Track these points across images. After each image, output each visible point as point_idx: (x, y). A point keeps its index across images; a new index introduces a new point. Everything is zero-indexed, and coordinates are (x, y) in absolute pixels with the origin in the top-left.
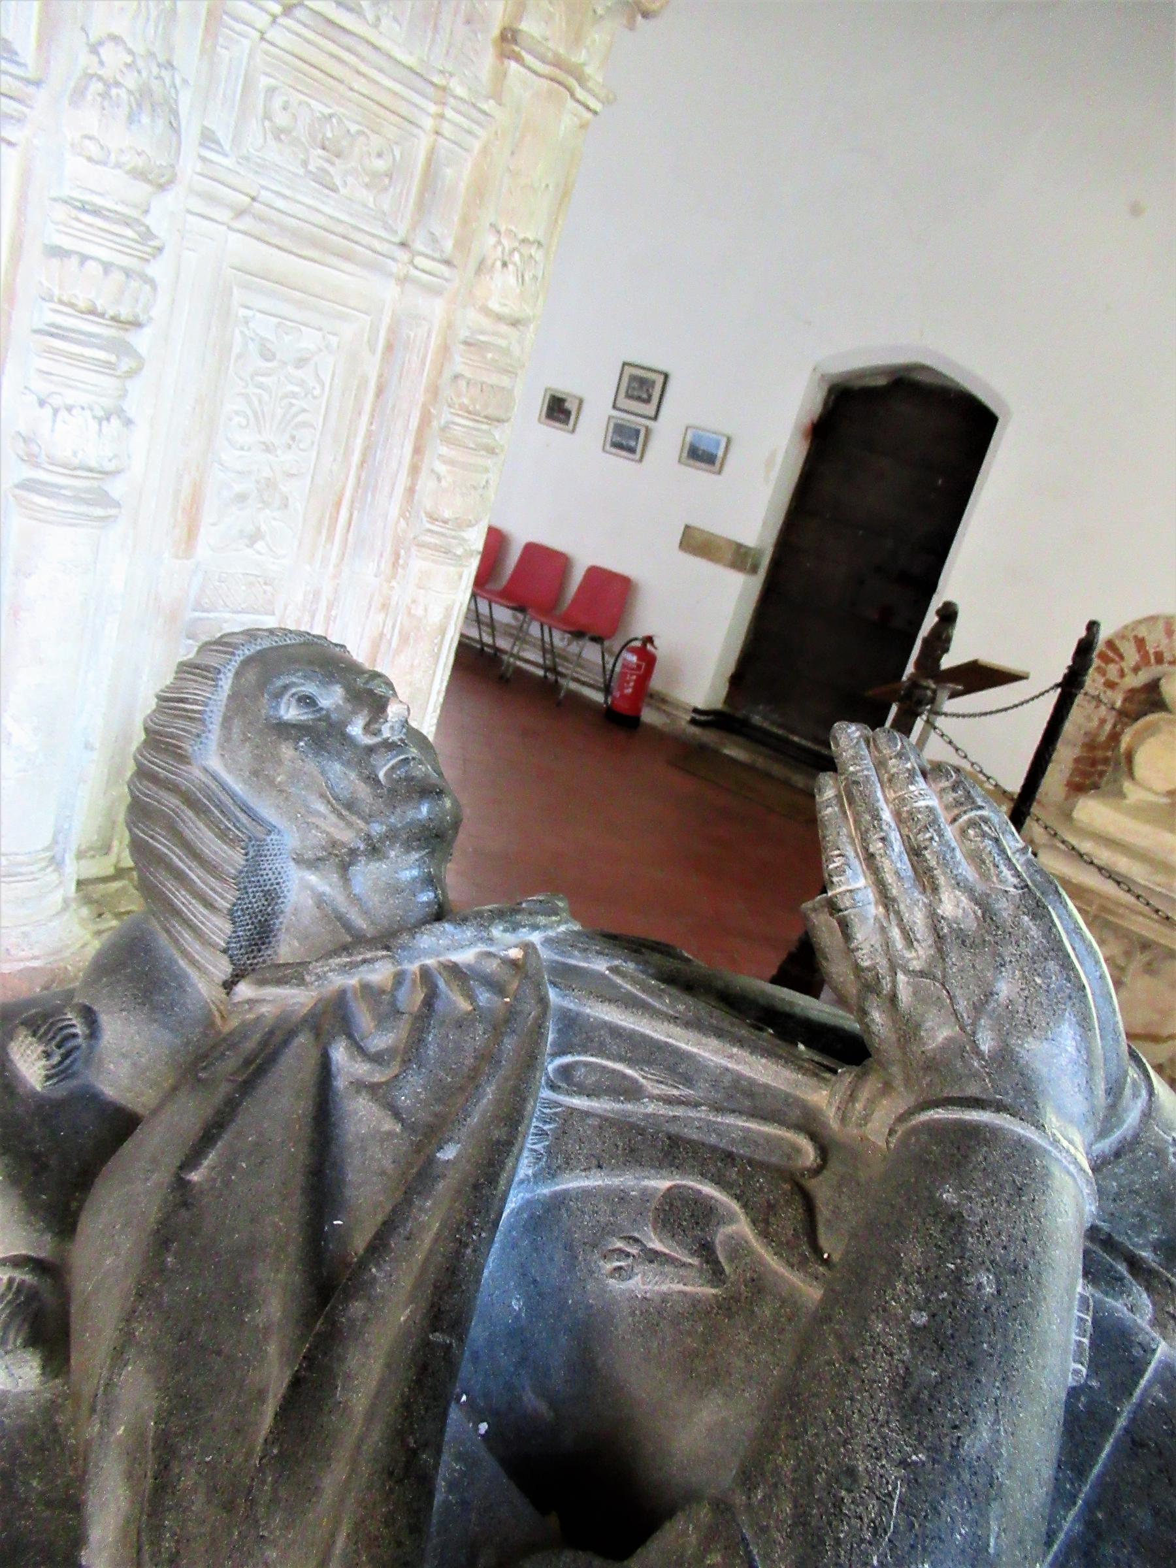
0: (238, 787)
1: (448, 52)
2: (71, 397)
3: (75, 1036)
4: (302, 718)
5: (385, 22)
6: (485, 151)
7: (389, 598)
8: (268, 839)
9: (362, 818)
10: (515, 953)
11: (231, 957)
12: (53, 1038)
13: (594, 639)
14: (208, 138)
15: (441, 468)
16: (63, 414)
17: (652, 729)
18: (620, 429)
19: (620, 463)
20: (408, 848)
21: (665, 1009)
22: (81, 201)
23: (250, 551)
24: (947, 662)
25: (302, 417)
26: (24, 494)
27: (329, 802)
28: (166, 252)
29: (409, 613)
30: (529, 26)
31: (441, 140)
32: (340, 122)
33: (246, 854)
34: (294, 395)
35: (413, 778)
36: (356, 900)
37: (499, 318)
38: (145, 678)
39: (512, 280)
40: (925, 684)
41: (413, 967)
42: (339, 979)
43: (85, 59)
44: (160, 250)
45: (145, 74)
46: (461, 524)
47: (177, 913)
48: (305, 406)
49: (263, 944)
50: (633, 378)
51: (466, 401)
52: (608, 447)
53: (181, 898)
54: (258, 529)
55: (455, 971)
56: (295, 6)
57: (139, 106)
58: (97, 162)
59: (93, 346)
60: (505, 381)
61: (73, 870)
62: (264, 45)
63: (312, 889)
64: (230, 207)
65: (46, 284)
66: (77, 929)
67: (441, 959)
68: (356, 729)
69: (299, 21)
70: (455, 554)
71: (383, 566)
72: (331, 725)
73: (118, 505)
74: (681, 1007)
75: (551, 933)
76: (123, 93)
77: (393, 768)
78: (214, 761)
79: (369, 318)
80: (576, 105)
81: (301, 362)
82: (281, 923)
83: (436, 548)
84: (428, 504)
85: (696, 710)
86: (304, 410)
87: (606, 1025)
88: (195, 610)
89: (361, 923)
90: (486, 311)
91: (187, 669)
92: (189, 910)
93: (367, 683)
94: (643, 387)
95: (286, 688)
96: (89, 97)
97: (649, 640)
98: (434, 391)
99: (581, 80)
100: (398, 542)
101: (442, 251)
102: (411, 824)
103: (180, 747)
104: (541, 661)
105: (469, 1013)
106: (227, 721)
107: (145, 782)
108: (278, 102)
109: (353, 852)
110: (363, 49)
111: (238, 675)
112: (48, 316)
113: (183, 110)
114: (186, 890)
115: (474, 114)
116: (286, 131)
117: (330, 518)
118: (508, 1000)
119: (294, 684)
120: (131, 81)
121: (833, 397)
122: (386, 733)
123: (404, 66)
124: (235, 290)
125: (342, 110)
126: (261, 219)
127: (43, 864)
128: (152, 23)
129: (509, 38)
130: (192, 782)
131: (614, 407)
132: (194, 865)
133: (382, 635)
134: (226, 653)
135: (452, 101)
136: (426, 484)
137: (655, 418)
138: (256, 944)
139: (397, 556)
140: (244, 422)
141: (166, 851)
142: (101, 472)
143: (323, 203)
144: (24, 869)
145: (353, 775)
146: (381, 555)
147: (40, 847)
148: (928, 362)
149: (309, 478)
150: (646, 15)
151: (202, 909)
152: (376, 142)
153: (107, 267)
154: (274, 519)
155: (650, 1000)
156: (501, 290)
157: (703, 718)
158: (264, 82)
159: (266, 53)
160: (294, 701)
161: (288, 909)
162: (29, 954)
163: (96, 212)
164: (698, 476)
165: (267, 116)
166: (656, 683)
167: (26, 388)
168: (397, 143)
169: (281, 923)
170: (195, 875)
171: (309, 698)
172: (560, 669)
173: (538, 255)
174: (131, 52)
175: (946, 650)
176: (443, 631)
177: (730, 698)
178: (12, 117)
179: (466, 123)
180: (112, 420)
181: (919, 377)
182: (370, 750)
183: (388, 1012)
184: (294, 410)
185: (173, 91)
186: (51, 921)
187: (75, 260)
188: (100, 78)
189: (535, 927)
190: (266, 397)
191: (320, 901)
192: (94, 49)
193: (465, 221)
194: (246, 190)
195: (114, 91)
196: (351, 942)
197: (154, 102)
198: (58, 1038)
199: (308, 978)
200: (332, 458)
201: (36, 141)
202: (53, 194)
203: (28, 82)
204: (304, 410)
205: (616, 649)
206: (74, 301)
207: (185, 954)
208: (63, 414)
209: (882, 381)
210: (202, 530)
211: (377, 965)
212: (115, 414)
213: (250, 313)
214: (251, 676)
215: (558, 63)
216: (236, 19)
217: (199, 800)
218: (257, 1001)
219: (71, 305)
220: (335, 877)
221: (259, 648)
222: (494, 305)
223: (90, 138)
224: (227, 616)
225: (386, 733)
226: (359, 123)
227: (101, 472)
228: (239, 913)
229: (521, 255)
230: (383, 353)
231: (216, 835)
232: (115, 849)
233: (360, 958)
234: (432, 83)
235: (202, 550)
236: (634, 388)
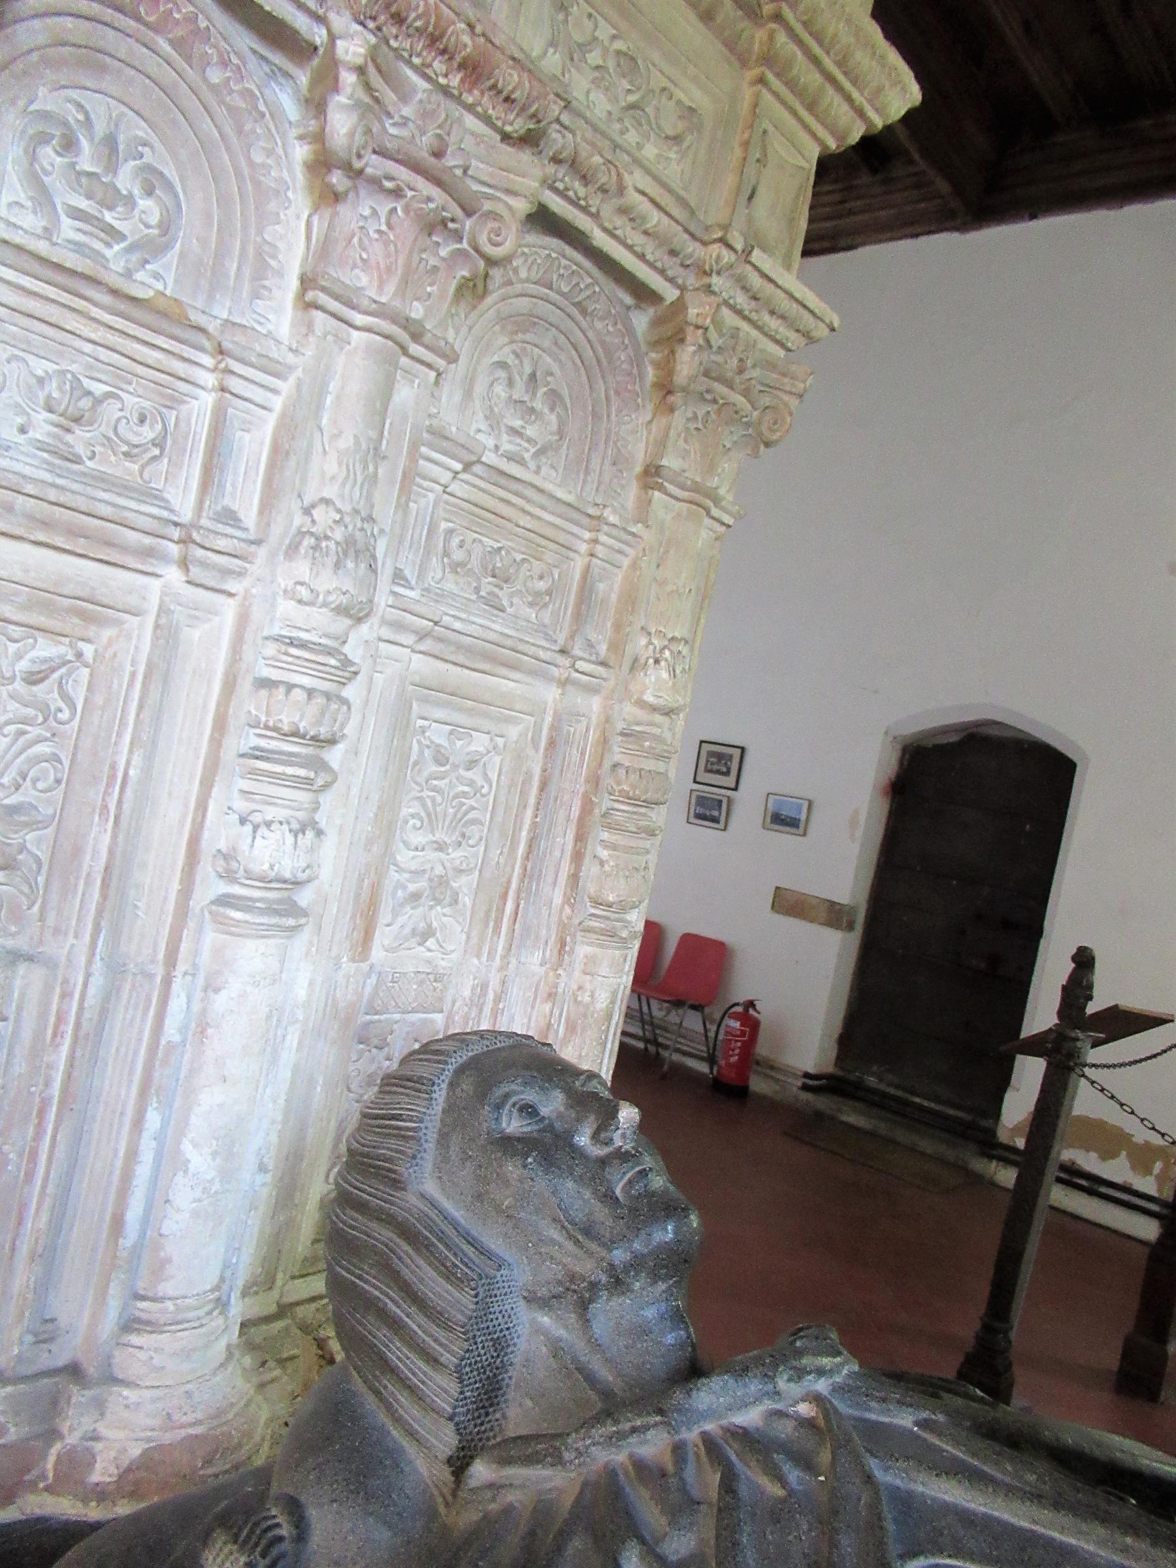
0: (458, 1214)
1: (597, 490)
2: (271, 813)
3: (280, 1539)
4: (525, 1129)
5: (544, 470)
6: (634, 566)
7: (556, 986)
8: (499, 1274)
9: (604, 1245)
10: (805, 1409)
11: (457, 1424)
12: (257, 1545)
13: (694, 1007)
14: (398, 576)
15: (604, 854)
16: (263, 830)
17: (762, 1098)
18: (702, 801)
19: (706, 834)
20: (655, 1278)
21: (1008, 1480)
22: (290, 638)
23: (422, 949)
24: (1091, 1008)
25: (472, 815)
26: (221, 910)
27: (563, 1227)
28: (359, 677)
29: (576, 1000)
30: (670, 462)
31: (594, 560)
32: (508, 552)
33: (476, 1296)
34: (465, 795)
35: (653, 1194)
36: (596, 1346)
37: (654, 709)
38: (319, 1089)
39: (665, 675)
40: (1073, 1035)
41: (691, 1435)
42: (602, 1454)
43: (298, 519)
44: (356, 673)
45: (350, 528)
46: (624, 907)
47: (393, 1371)
49: (491, 1405)
50: (711, 754)
51: (625, 788)
52: (692, 820)
53: (397, 1352)
54: (430, 926)
55: (743, 1436)
56: (473, 463)
57: (346, 554)
58: (306, 604)
59: (292, 764)
60: (661, 766)
61: (238, 1309)
62: (446, 496)
63: (546, 1333)
64: (415, 632)
65: (254, 712)
66: (240, 1382)
67: (724, 1422)
68: (583, 1139)
69: (477, 475)
70: (621, 938)
71: (548, 953)
72: (557, 1136)
73: (305, 913)
74: (1032, 1478)
75: (838, 1379)
76: (332, 545)
77: (630, 1182)
78: (430, 1184)
79: (532, 719)
80: (711, 521)
81: (471, 764)
82: (510, 1378)
83: (602, 932)
84: (592, 889)
85: (807, 1075)
86: (473, 808)
87: (948, 1509)
88: (367, 1014)
89: (606, 1375)
90: (641, 704)
91: (393, 1082)
92: (405, 1365)
93: (582, 1086)
94: (721, 761)
95: (507, 1096)
96: (303, 551)
97: (751, 1004)
98: (595, 781)
99: (717, 501)
100: (563, 927)
101: (597, 654)
102: (659, 1247)
103: (394, 1172)
104: (641, 1033)
105: (783, 1501)
106: (443, 1139)
107: (349, 1211)
108: (455, 541)
109: (594, 1286)
110: (529, 492)
111: (451, 1085)
112: (253, 740)
113: (380, 554)
114: (402, 1340)
115: (625, 537)
116: (461, 564)
117: (497, 909)
118: (822, 1478)
119: (515, 1093)
120: (338, 534)
121: (907, 756)
122: (618, 1142)
123: (565, 503)
124: (415, 705)
125: (510, 544)
126: (440, 640)
127: (210, 1306)
128: (357, 489)
129: (652, 475)
130: (409, 1211)
131: (695, 782)
132: (413, 1310)
133: (549, 1025)
134: (439, 1062)
135: (606, 528)
136: (589, 870)
137: (736, 789)
138: (483, 1407)
139: (563, 944)
140: (418, 824)
141: (377, 1293)
142: (293, 883)
143: (494, 621)
144: (191, 1315)
145: (587, 1194)
146: (547, 942)
147: (208, 1287)
148: (998, 718)
149: (477, 873)
150: (767, 445)
151: (421, 1364)
152: (538, 567)
153: (310, 693)
154: (445, 915)
155: (985, 1468)
156: (655, 684)
157: (816, 1083)
158: (444, 525)
159: (447, 503)
160: (515, 1110)
161: (517, 1359)
162: (190, 1418)
163: (303, 645)
164: (784, 839)
165: (446, 554)
166: (762, 1049)
167: (229, 808)
168: (555, 566)
169: (510, 1378)
170: (415, 1322)
171: (531, 1107)
172: (660, 1040)
173: (685, 651)
174: (339, 511)
175: (1090, 998)
176: (609, 1017)
177: (840, 1059)
178: (233, 572)
179: (617, 545)
180: (307, 832)
181: (995, 732)
182: (603, 1162)
183: (682, 1506)
184: (464, 808)
185: (372, 540)
186: (214, 1374)
187: (282, 689)
188: (312, 534)
189: (821, 1372)
190: (439, 799)
191: (556, 1349)
192: (307, 511)
193: (618, 627)
194: (430, 617)
195: (324, 544)
196: (612, 1405)
197: (357, 550)
198: (264, 1542)
199: (567, 1456)
201: (254, 591)
202: (265, 634)
203: (252, 542)
204: (473, 808)
205: (717, 1016)
206: (280, 725)
207: (398, 1420)
208: (263, 830)
209: (954, 738)
210: (377, 932)
211: (650, 1434)
212: (308, 826)
213: (426, 723)
214: (467, 1086)
215: (696, 488)
216: (425, 478)
217: (420, 1232)
218: (502, 1487)
219: (275, 729)
220: (573, 1318)
221: (470, 1054)
222: (649, 698)
223: (302, 584)
224: (397, 1016)
225: (618, 1142)
226: (523, 553)
227: (293, 883)
228: (468, 1369)
229: (672, 652)
230: (546, 749)
231: (440, 1273)
232: (279, 1283)
233: (627, 1426)
234: (589, 516)
235: (377, 954)
236: (712, 764)
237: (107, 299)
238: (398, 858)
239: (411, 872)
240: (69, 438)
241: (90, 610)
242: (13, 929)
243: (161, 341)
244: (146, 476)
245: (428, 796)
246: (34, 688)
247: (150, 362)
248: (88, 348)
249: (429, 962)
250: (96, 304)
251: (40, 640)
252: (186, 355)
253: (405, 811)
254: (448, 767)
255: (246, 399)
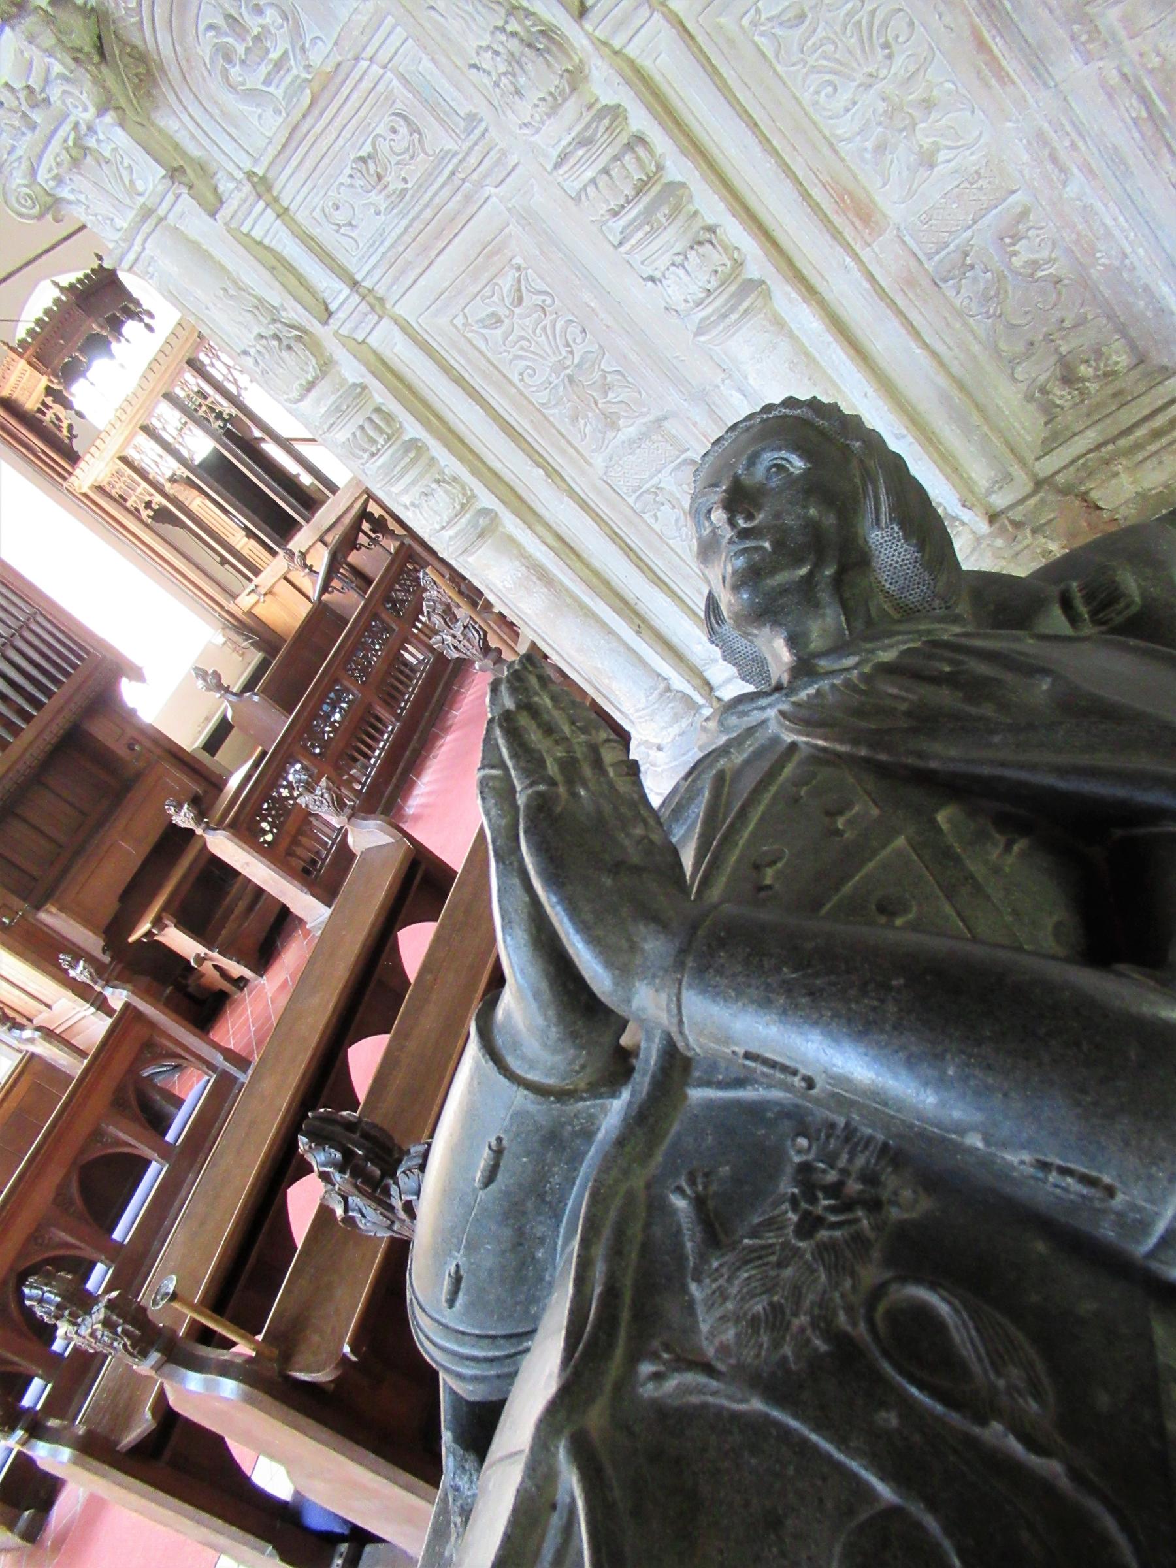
48: (870, 8)
86: (873, 13)
124: (722, 20)
128: (477, 17)
140: (830, 89)
184: (864, 22)
200: (937, 17)
204: (873, 13)
237: (310, 120)
238: (839, 132)
239: (858, 134)
240: (391, 188)
241: (491, 249)
242: (645, 410)
243: (345, 91)
244: (430, 152)
245: (817, 60)
246: (524, 304)
247: (357, 105)
248: (341, 141)
249: (956, 171)
250: (313, 127)
251: (500, 282)
252: (357, 78)
253: (806, 98)
254: (810, 16)
255: (396, 53)
